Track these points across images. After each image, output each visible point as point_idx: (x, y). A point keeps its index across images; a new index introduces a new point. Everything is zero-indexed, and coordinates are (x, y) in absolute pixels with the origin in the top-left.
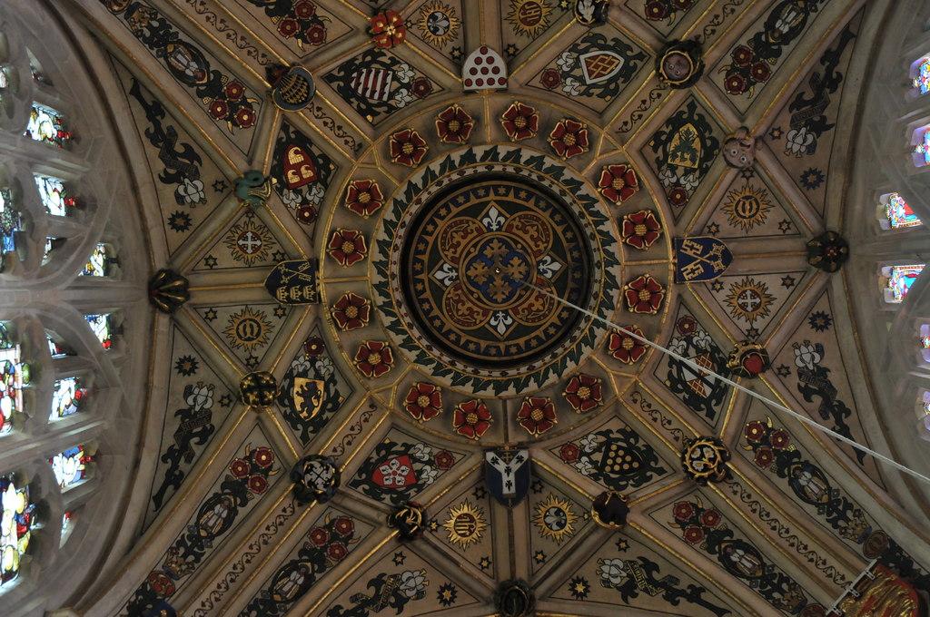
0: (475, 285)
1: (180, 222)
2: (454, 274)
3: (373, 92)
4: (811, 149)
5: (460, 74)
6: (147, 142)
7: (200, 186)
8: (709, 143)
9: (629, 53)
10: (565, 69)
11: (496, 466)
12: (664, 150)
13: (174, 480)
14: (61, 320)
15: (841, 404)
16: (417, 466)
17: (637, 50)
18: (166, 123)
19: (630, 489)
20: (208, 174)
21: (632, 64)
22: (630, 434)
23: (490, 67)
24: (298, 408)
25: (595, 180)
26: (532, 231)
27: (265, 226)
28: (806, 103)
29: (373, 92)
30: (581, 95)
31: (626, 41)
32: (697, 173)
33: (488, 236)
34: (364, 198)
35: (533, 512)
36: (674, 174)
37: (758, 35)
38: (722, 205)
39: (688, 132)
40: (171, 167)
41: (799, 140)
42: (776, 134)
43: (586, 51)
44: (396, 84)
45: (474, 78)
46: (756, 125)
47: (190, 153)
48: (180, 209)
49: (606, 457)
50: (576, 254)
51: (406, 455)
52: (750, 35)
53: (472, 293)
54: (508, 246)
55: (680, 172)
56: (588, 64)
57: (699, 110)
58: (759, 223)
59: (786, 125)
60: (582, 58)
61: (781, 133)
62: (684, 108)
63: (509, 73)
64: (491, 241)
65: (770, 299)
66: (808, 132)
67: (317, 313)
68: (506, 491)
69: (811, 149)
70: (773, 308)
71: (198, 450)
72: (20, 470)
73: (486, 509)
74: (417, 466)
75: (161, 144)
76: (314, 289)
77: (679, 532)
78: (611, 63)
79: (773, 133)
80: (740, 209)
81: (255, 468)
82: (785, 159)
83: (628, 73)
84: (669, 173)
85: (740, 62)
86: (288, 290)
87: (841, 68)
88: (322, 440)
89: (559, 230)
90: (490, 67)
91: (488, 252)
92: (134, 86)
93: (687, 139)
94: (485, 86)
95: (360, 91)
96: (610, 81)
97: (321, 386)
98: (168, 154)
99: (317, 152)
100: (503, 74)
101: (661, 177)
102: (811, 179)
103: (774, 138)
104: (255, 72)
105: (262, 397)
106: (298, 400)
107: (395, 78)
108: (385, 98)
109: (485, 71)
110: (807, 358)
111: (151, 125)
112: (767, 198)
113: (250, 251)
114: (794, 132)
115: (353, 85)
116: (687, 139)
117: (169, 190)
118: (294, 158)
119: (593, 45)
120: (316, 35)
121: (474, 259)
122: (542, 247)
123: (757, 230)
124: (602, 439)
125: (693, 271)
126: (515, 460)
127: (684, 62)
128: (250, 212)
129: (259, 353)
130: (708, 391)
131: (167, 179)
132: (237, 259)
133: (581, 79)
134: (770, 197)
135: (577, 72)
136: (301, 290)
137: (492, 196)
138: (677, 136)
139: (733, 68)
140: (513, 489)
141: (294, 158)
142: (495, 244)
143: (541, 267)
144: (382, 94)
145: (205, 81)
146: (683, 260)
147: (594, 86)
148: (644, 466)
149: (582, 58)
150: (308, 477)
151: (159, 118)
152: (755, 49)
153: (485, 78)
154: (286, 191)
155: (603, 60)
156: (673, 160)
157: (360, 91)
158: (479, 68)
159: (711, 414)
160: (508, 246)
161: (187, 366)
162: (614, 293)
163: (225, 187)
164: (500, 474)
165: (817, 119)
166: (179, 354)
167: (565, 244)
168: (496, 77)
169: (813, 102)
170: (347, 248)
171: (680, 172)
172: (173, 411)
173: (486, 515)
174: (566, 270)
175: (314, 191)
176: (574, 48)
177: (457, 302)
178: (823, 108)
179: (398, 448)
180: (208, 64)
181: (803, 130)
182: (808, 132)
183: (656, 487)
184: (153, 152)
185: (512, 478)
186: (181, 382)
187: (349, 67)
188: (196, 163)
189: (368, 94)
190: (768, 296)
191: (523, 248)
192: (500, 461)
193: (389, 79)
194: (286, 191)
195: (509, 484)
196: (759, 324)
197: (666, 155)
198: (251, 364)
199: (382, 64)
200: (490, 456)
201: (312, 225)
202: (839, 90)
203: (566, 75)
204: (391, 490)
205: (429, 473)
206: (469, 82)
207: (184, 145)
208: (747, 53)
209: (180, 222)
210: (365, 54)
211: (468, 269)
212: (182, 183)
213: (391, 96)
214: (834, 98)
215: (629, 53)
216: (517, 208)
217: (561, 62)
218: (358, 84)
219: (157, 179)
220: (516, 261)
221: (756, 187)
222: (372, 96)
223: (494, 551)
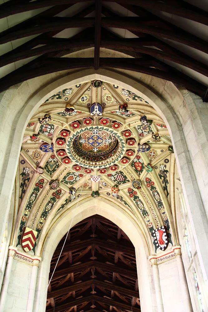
0: (101, 139)
1: (167, 161)
2: (106, 141)
3: (120, 176)
4: (24, 169)
6: (169, 181)
7: (160, 168)
8: (47, 168)
9: (65, 182)
10: (78, 177)
11: (99, 112)
12: (56, 165)
14: (183, 212)
17: (63, 182)
18: (163, 185)
20: (158, 171)
21: (64, 180)
23: (94, 179)
26: (86, 134)
27: (148, 157)
28: (27, 179)
29: (120, 176)
30: (75, 173)
31: (65, 184)
32: (49, 162)
34: (126, 159)
35: (90, 99)
36: (54, 161)
37: (38, 192)
38: (43, 156)
39: (51, 169)
40: (165, 174)
41: (27, 171)
42: (32, 172)
43: (74, 181)
44: (115, 176)
45: (98, 178)
46: (36, 175)
47: (161, 176)
48: (166, 164)
50: (76, 143)
52: (40, 191)
53: (102, 137)
54: (93, 145)
55: (53, 161)
56: (73, 178)
57: (49, 174)
58: (34, 152)
59: (30, 174)
60: (74, 179)
61: (31, 172)
62: (52, 173)
64: (96, 146)
66: (25, 173)
67: (139, 142)
68: (97, 107)
69: (24, 169)
73: (103, 100)
75: (166, 180)
76: (139, 147)
77: (128, 194)
78: (68, 179)
79: (34, 172)
80: (38, 155)
82: (29, 166)
83: (65, 178)
84: (55, 161)
85: (42, 185)
86: (145, 148)
87: (21, 189)
89: (80, 147)
91: (97, 144)
92: (168, 194)
93: (51, 168)
94: (96, 177)
95: (123, 177)
96: (68, 176)
98: (165, 177)
99: (134, 168)
101: (57, 160)
102: (23, 162)
103: (33, 171)
104: (143, 189)
107: (115, 178)
108: (117, 174)
111: (167, 185)
112: (32, 157)
113: (153, 152)
114: (28, 172)
115: (124, 178)
116: (51, 168)
117: (167, 169)
118: (139, 169)
119: (72, 182)
120: (130, 190)
121: (101, 143)
122: (84, 145)
123: (34, 150)
125: (49, 147)
126: (94, 113)
127: (54, 187)
128: (151, 161)
131: (167, 171)
132: (156, 151)
133: (75, 175)
134: (32, 158)
135: (76, 177)
136: (142, 147)
137: (96, 154)
138: (54, 168)
139: (43, 184)
140: (95, 107)
141: (139, 169)
142: (95, 145)
143: (85, 141)
144: (118, 175)
145: (154, 190)
146: (52, 148)
147: (72, 174)
149: (74, 179)
151: (165, 186)
152: (39, 189)
154: (142, 163)
155: (70, 179)
156: (54, 163)
157: (123, 177)
160: (93, 145)
162: (68, 144)
163: (155, 167)
164: (98, 111)
165: (24, 176)
167: (79, 145)
168: (93, 178)
169: (25, 180)
170: (61, 140)
171: (53, 161)
173: (103, 99)
174: (79, 140)
175: (136, 161)
176: (76, 181)
177: (106, 136)
178: (23, 179)
180: (153, 193)
181: (26, 173)
182: (25, 173)
184: (168, 179)
187: (124, 182)
188: (160, 174)
189: (121, 176)
191: (89, 145)
192: (98, 113)
193: (116, 178)
194: (142, 163)
195: (96, 108)
197: (56, 164)
199: (117, 181)
201: (138, 155)
202: (20, 184)
203: (78, 176)
207: (161, 179)
208: (40, 187)
209: (167, 161)
210: (120, 184)
211: (102, 142)
212: (164, 170)
213: (116, 174)
214: (21, 182)
215: (65, 182)
216: (90, 151)
217: (79, 179)
218: (123, 178)
219: (169, 172)
221: (35, 160)
222: (120, 175)
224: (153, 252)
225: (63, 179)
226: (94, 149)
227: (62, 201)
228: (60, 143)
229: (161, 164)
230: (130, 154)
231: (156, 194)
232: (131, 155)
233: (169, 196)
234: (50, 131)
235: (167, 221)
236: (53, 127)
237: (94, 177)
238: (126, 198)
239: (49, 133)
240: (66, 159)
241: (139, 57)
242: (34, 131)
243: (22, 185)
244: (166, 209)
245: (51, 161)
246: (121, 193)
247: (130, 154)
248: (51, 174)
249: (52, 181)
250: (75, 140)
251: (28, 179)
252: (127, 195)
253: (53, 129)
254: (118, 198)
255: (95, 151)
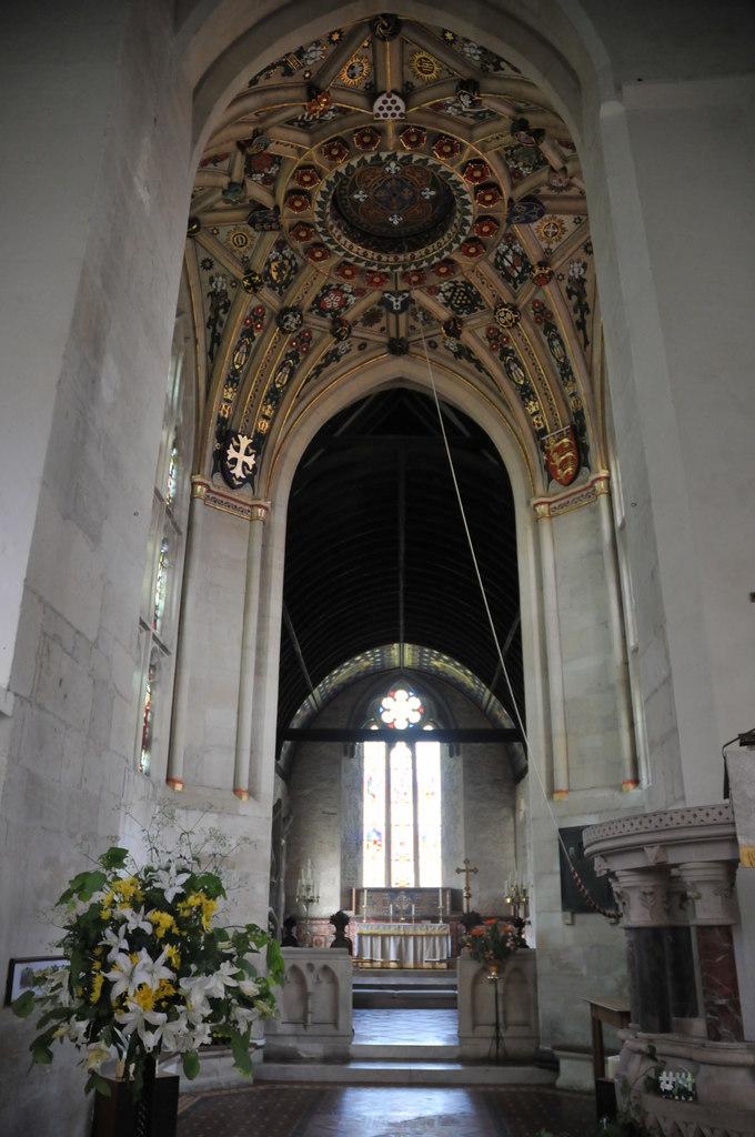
5: (372, 110)
13: (216, 340)
15: (587, 304)
16: (345, 295)
19: (464, 315)
22: (468, 284)
23: (393, 106)
24: (275, 277)
25: (463, 170)
33: (388, 177)
34: (475, 245)
41: (219, 284)
45: (381, 113)
49: (453, 295)
51: (339, 290)
55: (521, 164)
63: (407, 109)
65: (564, 230)
70: (564, 237)
71: (224, 317)
72: (355, 1130)
74: (345, 295)
77: (487, 343)
81: (256, 317)
87: (210, 331)
88: (291, 294)
90: (393, 106)
91: (389, 185)
97: (286, 262)
100: (403, 110)
105: (251, 281)
106: (274, 275)
109: (389, 108)
110: (576, 270)
111: (586, 317)
124: (451, 285)
129: (249, 254)
130: (516, 275)
148: (474, 304)
150: (287, 324)
153: (390, 113)
158: (385, 106)
159: (516, 287)
161: (208, 264)
166: (201, 258)
168: (398, 113)
169: (218, 308)
170: (298, 195)
172: (205, 294)
179: (334, 287)
180: (549, 340)
183: (478, 320)
185: (399, 303)
186: (206, 275)
190: (563, 229)
196: (554, 246)
198: (245, 263)
200: (386, 295)
204: (331, 310)
205: (352, 299)
206: (378, 115)
220: (406, 190)
223: (388, 325)
224: (540, 489)
225: (313, 304)
226: (399, 168)
227: (315, 358)
228: (298, 204)
229: (575, 257)
230: (485, 229)
231: (556, 343)
232: (488, 233)
233: (588, 348)
234: (507, 252)
235: (579, 415)
236: (499, 259)
237: (394, 115)
238: (482, 353)
239: (510, 247)
240: (317, 250)
241: (443, 111)
242: (230, 174)
243: (212, 323)
244: (582, 386)
245: (524, 166)
246: (467, 338)
247: (485, 229)
248: (281, 293)
249: (285, 311)
250: (334, 196)
251: (227, 306)
252: (484, 346)
253: (498, 254)
254: (458, 355)
255: (396, 222)
